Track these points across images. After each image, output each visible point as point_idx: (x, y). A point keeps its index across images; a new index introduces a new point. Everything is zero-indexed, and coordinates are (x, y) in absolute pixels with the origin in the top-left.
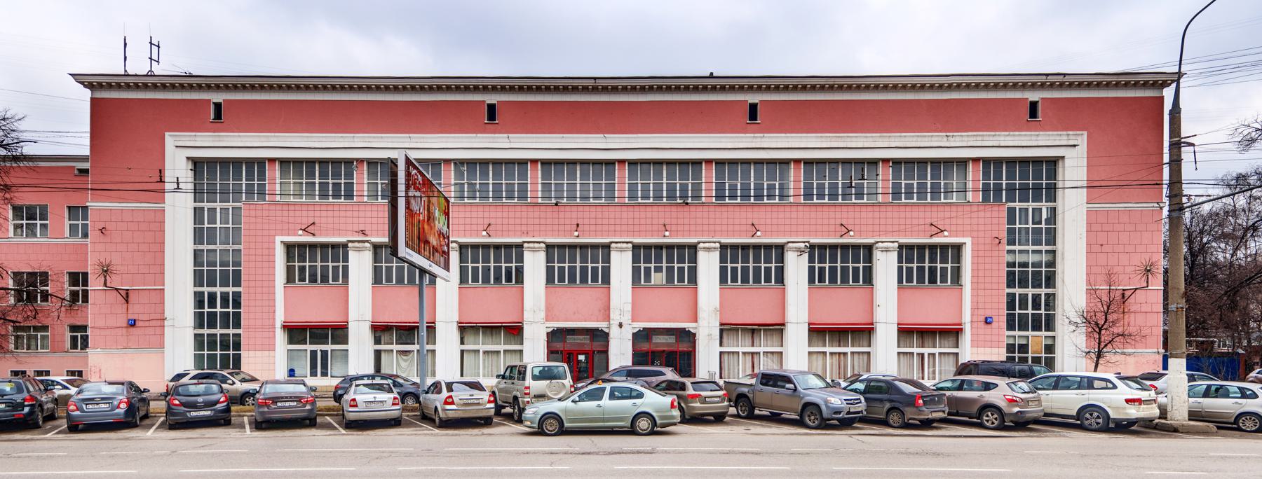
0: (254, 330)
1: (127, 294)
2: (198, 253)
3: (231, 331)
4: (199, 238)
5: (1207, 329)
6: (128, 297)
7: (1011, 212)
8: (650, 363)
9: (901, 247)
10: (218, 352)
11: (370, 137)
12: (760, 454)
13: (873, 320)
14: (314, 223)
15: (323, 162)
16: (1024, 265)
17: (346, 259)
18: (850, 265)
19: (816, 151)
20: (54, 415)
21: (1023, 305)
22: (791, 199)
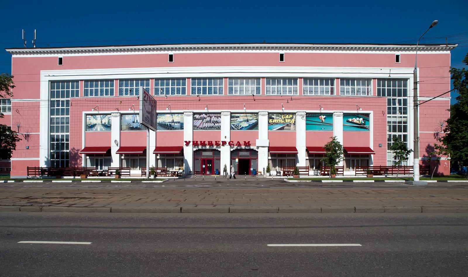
0: (391, 172)
2: (52, 119)
3: (65, 116)
4: (86, 93)
5: (6, 74)
7: (389, 100)
8: (218, 161)
10: (60, 125)
11: (286, 68)
12: (223, 182)
15: (102, 81)
16: (395, 122)
18: (176, 87)
20: (249, 167)
21: (178, 90)
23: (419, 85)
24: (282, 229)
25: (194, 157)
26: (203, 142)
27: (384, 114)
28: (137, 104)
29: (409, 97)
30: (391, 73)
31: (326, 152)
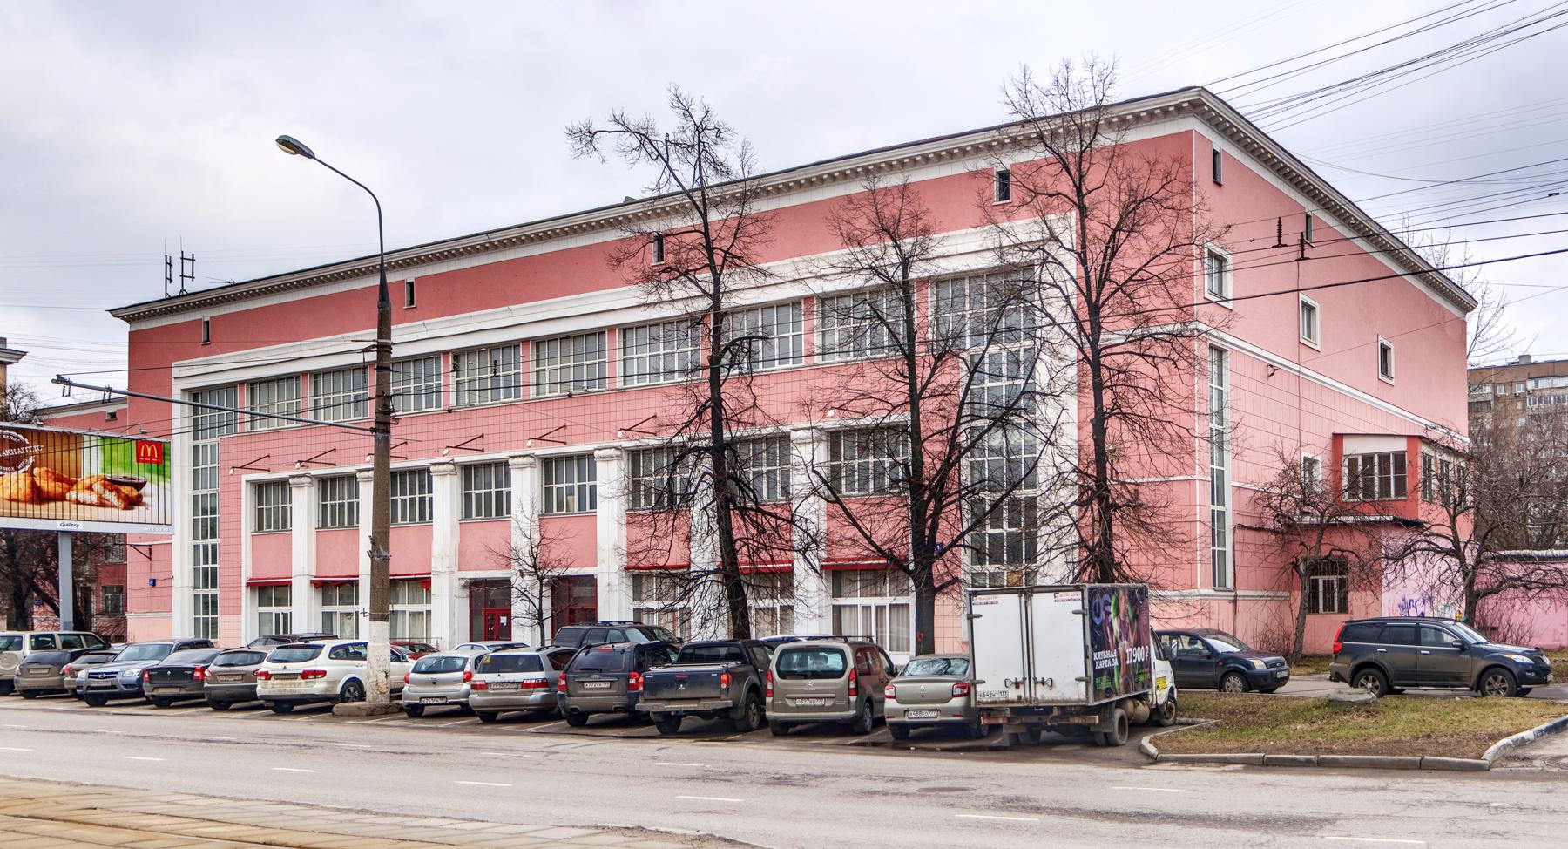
1: (150, 550)
6: (150, 553)
9: (897, 674)
13: (357, 568)
14: (335, 450)
17: (593, 476)
19: (618, 313)
22: (619, 384)
23: (170, 394)
24: (1342, 725)
25: (1439, 770)
26: (363, 652)
27: (387, 493)
28: (235, 527)
29: (384, 361)
30: (1300, 288)
31: (1503, 553)
